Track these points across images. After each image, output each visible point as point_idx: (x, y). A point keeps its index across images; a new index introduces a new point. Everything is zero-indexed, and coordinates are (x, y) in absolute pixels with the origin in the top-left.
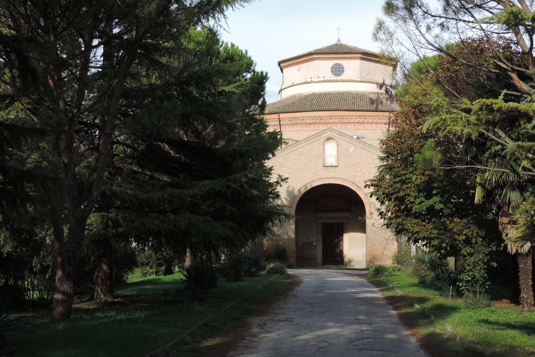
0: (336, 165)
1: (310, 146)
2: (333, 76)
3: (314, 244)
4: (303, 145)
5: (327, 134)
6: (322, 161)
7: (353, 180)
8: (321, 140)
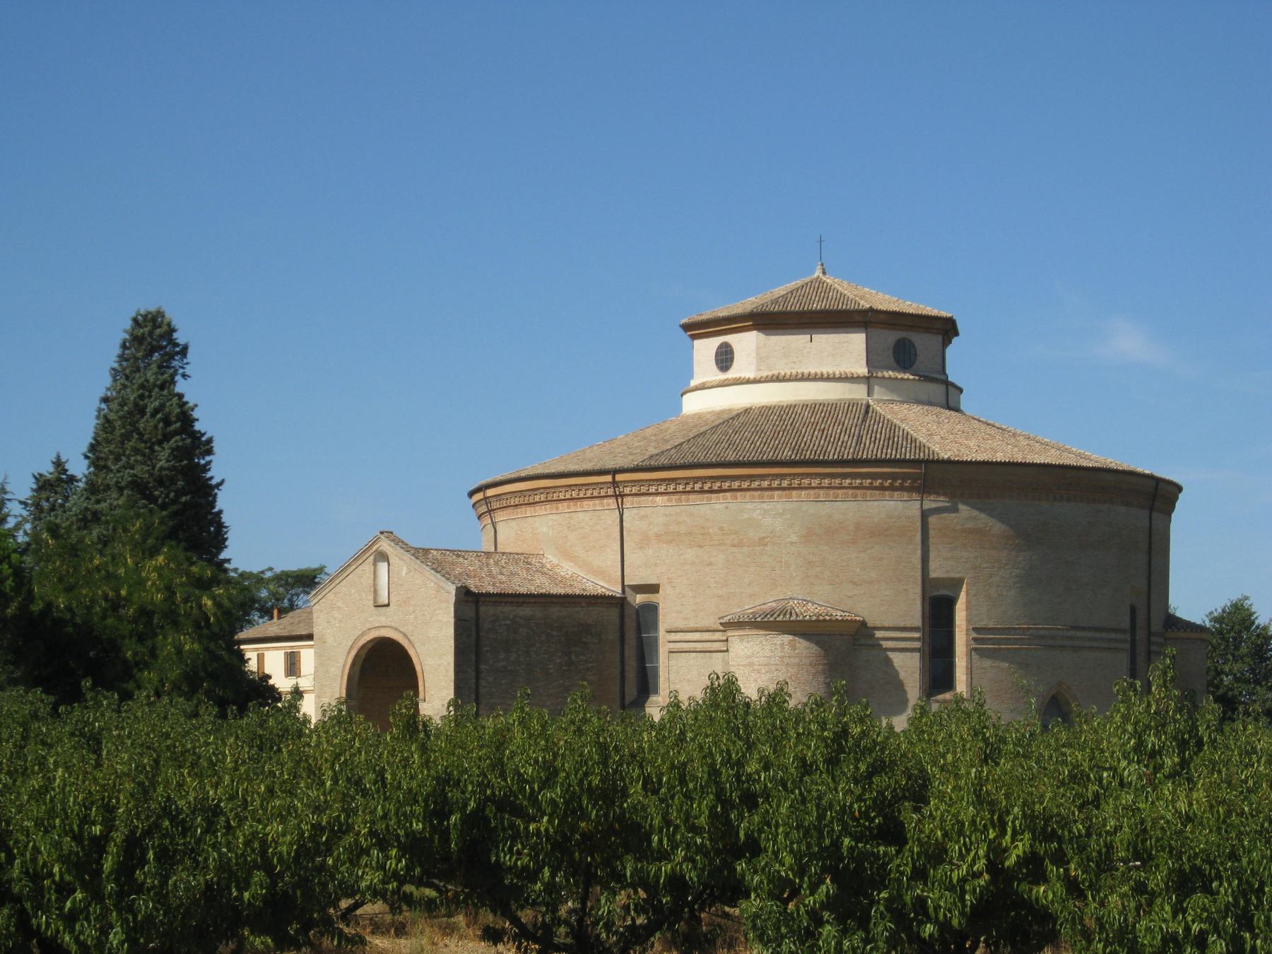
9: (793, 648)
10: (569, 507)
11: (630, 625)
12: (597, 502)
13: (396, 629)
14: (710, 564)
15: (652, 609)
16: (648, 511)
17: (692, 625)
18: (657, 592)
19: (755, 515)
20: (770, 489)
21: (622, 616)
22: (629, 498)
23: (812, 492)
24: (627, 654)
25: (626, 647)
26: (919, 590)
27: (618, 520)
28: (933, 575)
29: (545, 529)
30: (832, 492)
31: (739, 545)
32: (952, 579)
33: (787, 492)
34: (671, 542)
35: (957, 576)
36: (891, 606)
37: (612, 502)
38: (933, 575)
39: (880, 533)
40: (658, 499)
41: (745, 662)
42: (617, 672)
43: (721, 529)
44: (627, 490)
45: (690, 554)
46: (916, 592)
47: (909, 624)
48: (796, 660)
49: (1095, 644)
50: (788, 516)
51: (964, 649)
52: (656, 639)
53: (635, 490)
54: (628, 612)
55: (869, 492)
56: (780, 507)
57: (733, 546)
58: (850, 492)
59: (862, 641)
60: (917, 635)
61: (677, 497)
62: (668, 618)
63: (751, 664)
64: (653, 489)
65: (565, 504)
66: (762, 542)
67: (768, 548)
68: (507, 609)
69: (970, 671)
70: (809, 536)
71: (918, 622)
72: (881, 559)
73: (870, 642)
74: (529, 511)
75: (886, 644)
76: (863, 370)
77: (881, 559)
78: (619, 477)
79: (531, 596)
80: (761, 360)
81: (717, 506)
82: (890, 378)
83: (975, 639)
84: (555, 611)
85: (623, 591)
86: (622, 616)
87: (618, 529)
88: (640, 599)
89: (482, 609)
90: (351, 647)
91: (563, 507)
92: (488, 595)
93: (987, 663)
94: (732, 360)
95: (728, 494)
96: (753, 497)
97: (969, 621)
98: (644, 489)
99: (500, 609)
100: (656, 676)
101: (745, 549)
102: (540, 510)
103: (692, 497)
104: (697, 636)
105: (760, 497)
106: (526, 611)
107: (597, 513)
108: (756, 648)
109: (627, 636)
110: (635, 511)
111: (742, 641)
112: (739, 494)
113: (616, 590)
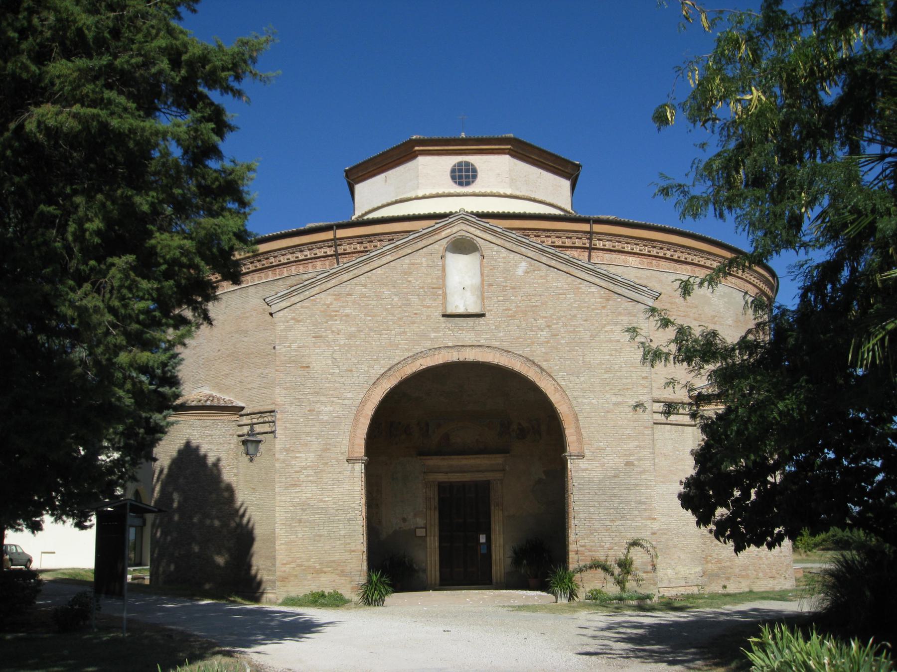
0: (473, 310)
1: (407, 260)
2: (454, 185)
3: (420, 533)
4: (389, 258)
5: (454, 230)
6: (439, 301)
7: (526, 352)
8: (436, 246)
22: (600, 253)
40: (631, 259)
44: (599, 245)
64: (628, 248)
78: (597, 228)
98: (618, 246)
103: (663, 263)
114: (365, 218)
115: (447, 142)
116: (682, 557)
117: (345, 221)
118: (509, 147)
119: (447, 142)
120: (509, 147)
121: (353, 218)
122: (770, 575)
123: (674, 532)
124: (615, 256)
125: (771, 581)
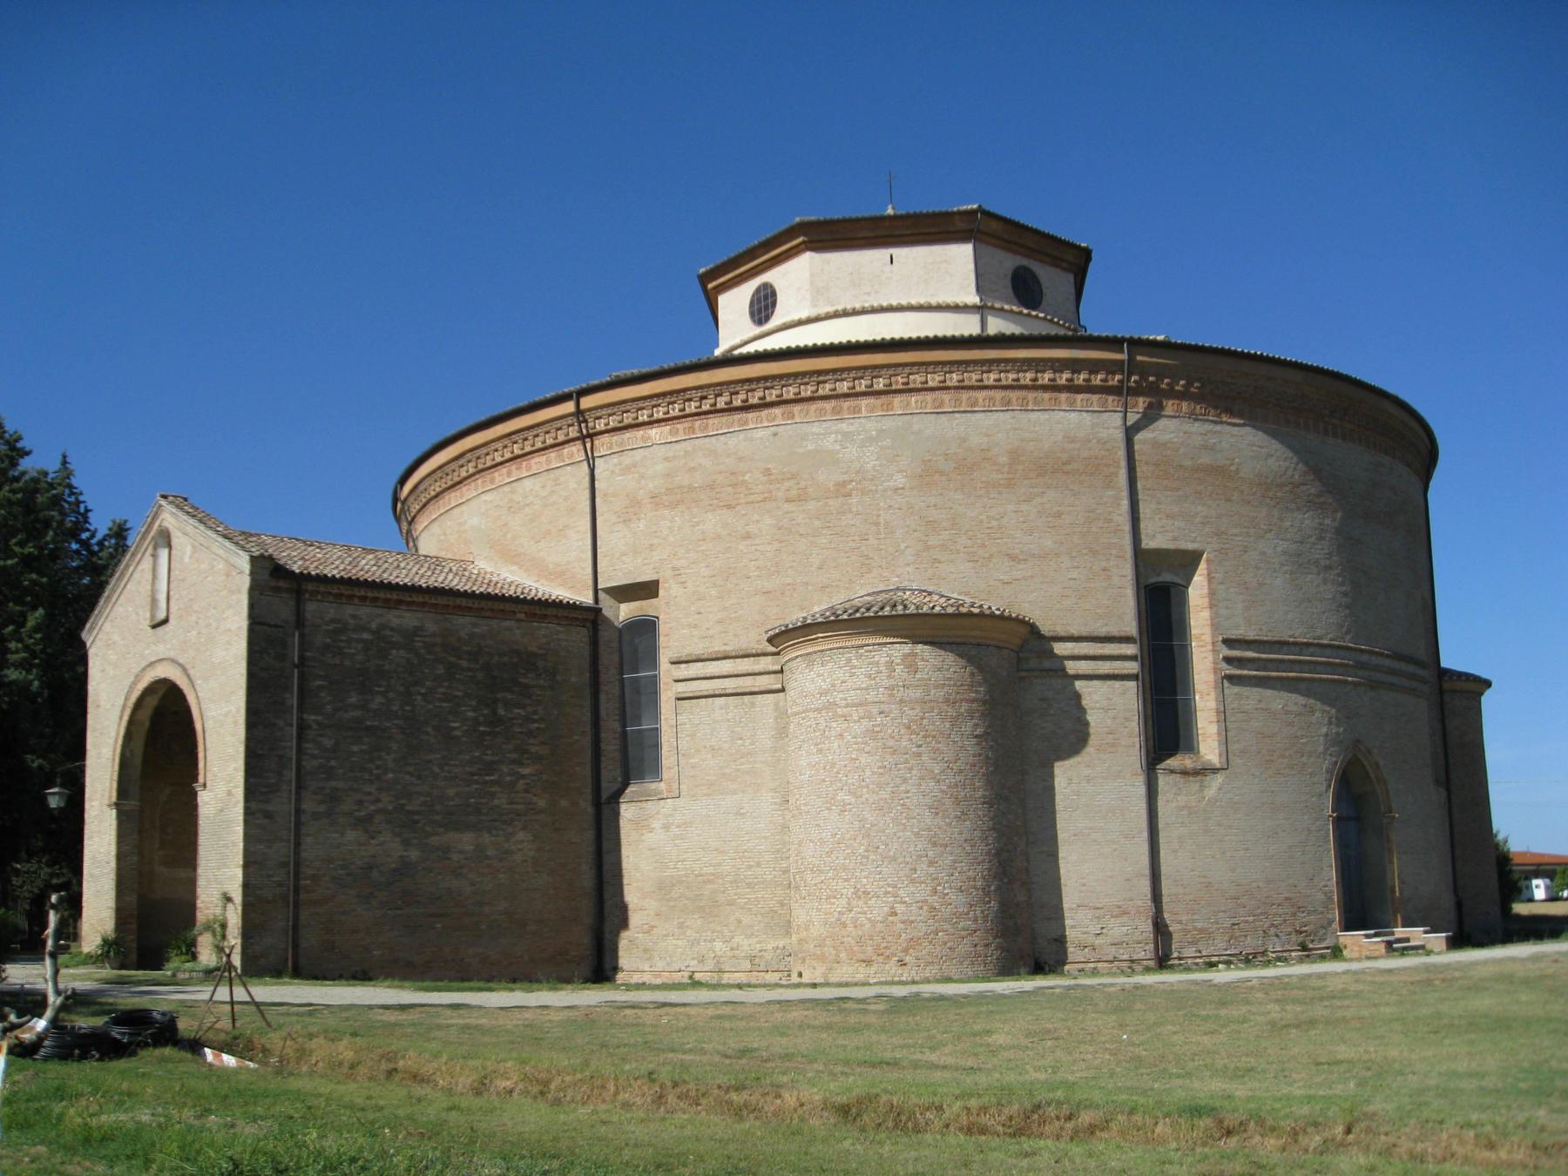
9: (912, 668)
10: (509, 474)
11: (608, 658)
12: (553, 454)
13: (185, 670)
14: (748, 536)
15: (646, 628)
16: (638, 455)
17: (718, 647)
18: (655, 594)
19: (829, 443)
20: (852, 395)
21: (594, 642)
22: (605, 438)
23: (929, 397)
24: (603, 712)
25: (603, 697)
26: (1128, 570)
27: (587, 480)
28: (1148, 543)
29: (475, 521)
30: (965, 395)
31: (801, 498)
32: (1184, 553)
33: (884, 399)
34: (678, 503)
35: (1190, 546)
36: (1079, 600)
37: (575, 451)
38: (1144, 545)
39: (1053, 468)
40: (654, 433)
41: (818, 704)
42: (587, 741)
43: (767, 472)
44: (600, 425)
45: (712, 522)
46: (1125, 573)
47: (1114, 630)
48: (918, 694)
49: (1395, 680)
50: (888, 442)
51: (1211, 678)
52: (654, 682)
53: (613, 422)
54: (604, 635)
55: (1031, 395)
56: (872, 426)
57: (788, 500)
58: (998, 394)
59: (1033, 663)
60: (1130, 649)
61: (686, 424)
62: (670, 644)
63: (831, 706)
64: (644, 417)
65: (504, 470)
66: (842, 489)
67: (854, 500)
68: (365, 611)
69: (1223, 715)
70: (927, 476)
71: (1131, 627)
72: (1059, 515)
73: (1047, 664)
74: (453, 498)
75: (1072, 667)
76: (973, 299)
77: (1059, 515)
78: (587, 402)
79: (414, 589)
80: (817, 292)
81: (760, 434)
82: (1012, 311)
83: (1228, 660)
84: (463, 624)
85: (596, 600)
86: (594, 642)
87: (587, 494)
88: (625, 612)
89: (311, 607)
90: (124, 707)
91: (500, 476)
92: (323, 579)
93: (1253, 695)
94: (774, 304)
95: (777, 411)
96: (822, 411)
97: (1215, 626)
98: (628, 419)
99: (349, 610)
100: (656, 746)
101: (812, 505)
102: (467, 491)
103: (714, 421)
104: (726, 666)
105: (834, 411)
106: (405, 619)
107: (552, 475)
108: (840, 674)
109: (603, 677)
110: (615, 459)
111: (811, 664)
112: (797, 408)
113: (587, 598)
114: (736, 352)
115: (751, 254)
116: (746, 920)
117: (704, 359)
118: (801, 239)
119: (751, 254)
120: (801, 239)
121: (717, 352)
122: (862, 957)
123: (729, 878)
124: (627, 435)
125: (862, 969)
